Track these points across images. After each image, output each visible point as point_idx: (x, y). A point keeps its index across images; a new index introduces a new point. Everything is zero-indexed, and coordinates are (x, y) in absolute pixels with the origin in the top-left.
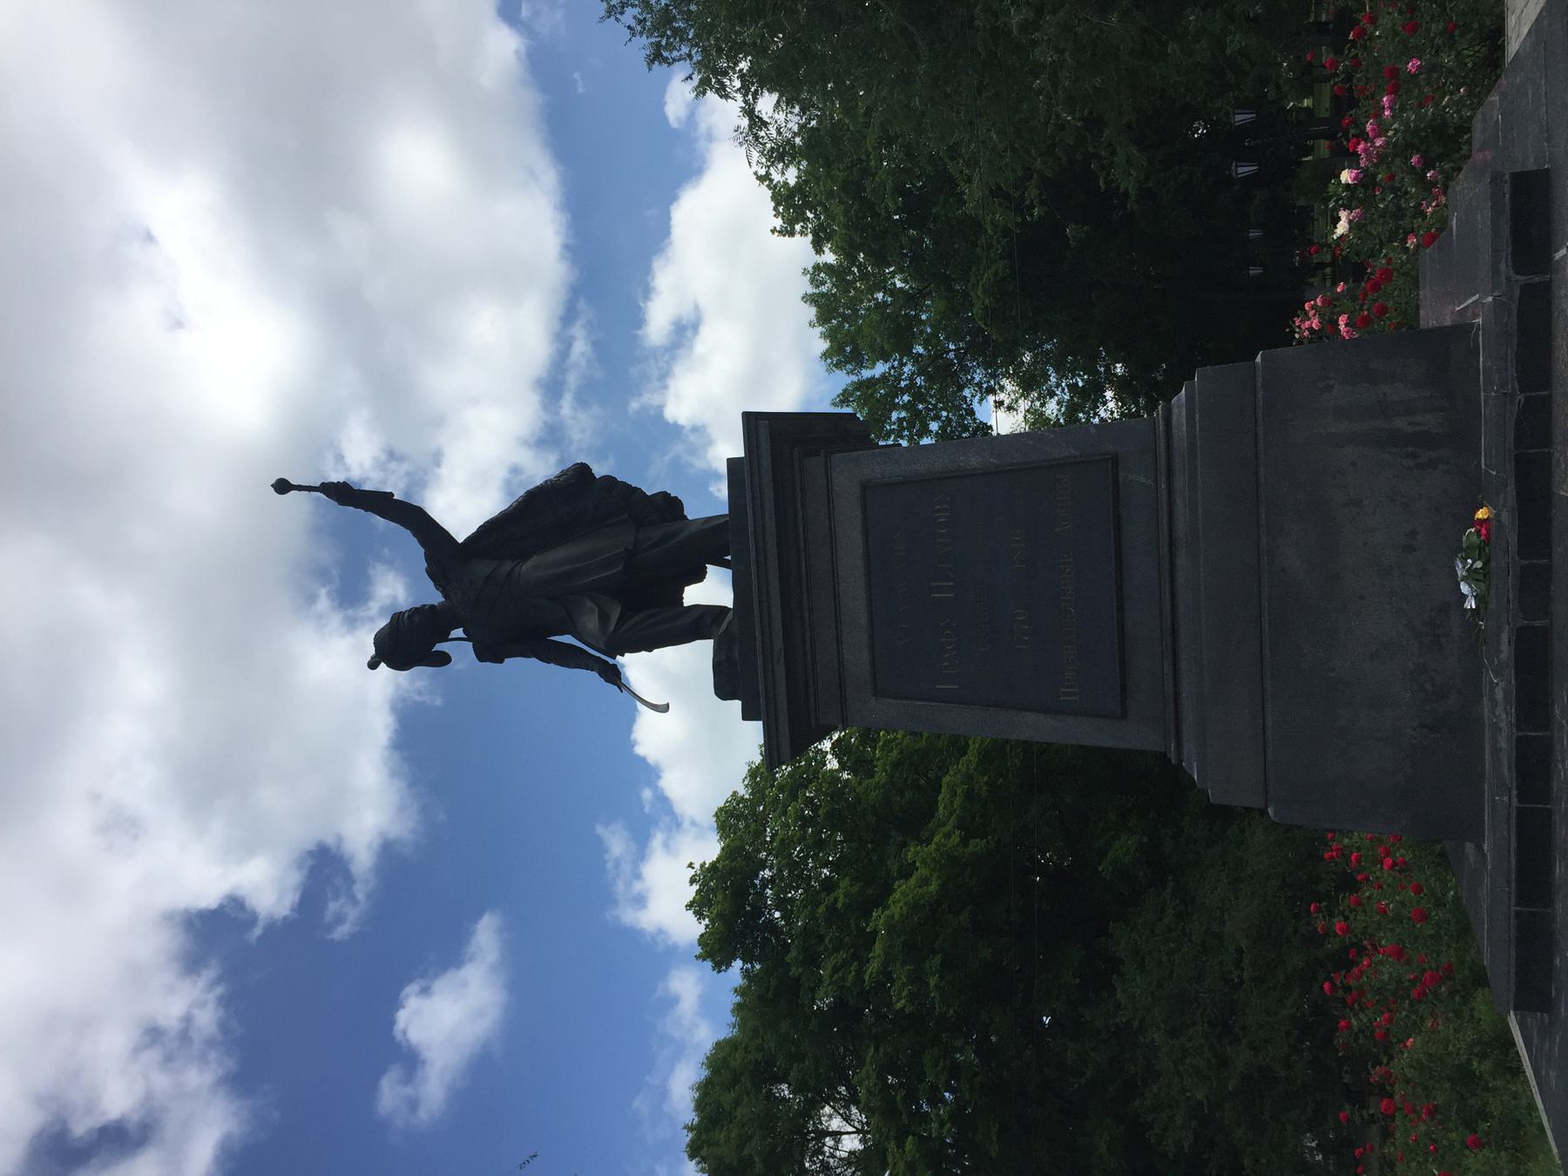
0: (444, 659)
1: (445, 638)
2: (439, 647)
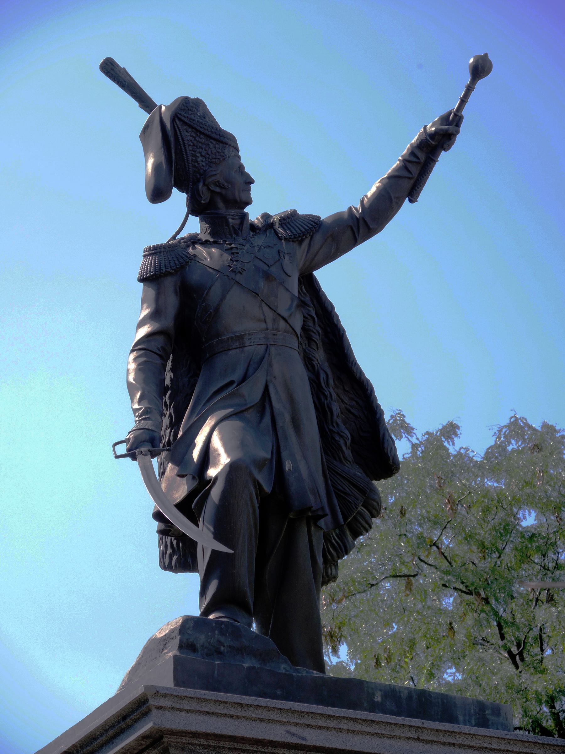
0: (158, 194)
1: (195, 208)
2: (178, 199)
